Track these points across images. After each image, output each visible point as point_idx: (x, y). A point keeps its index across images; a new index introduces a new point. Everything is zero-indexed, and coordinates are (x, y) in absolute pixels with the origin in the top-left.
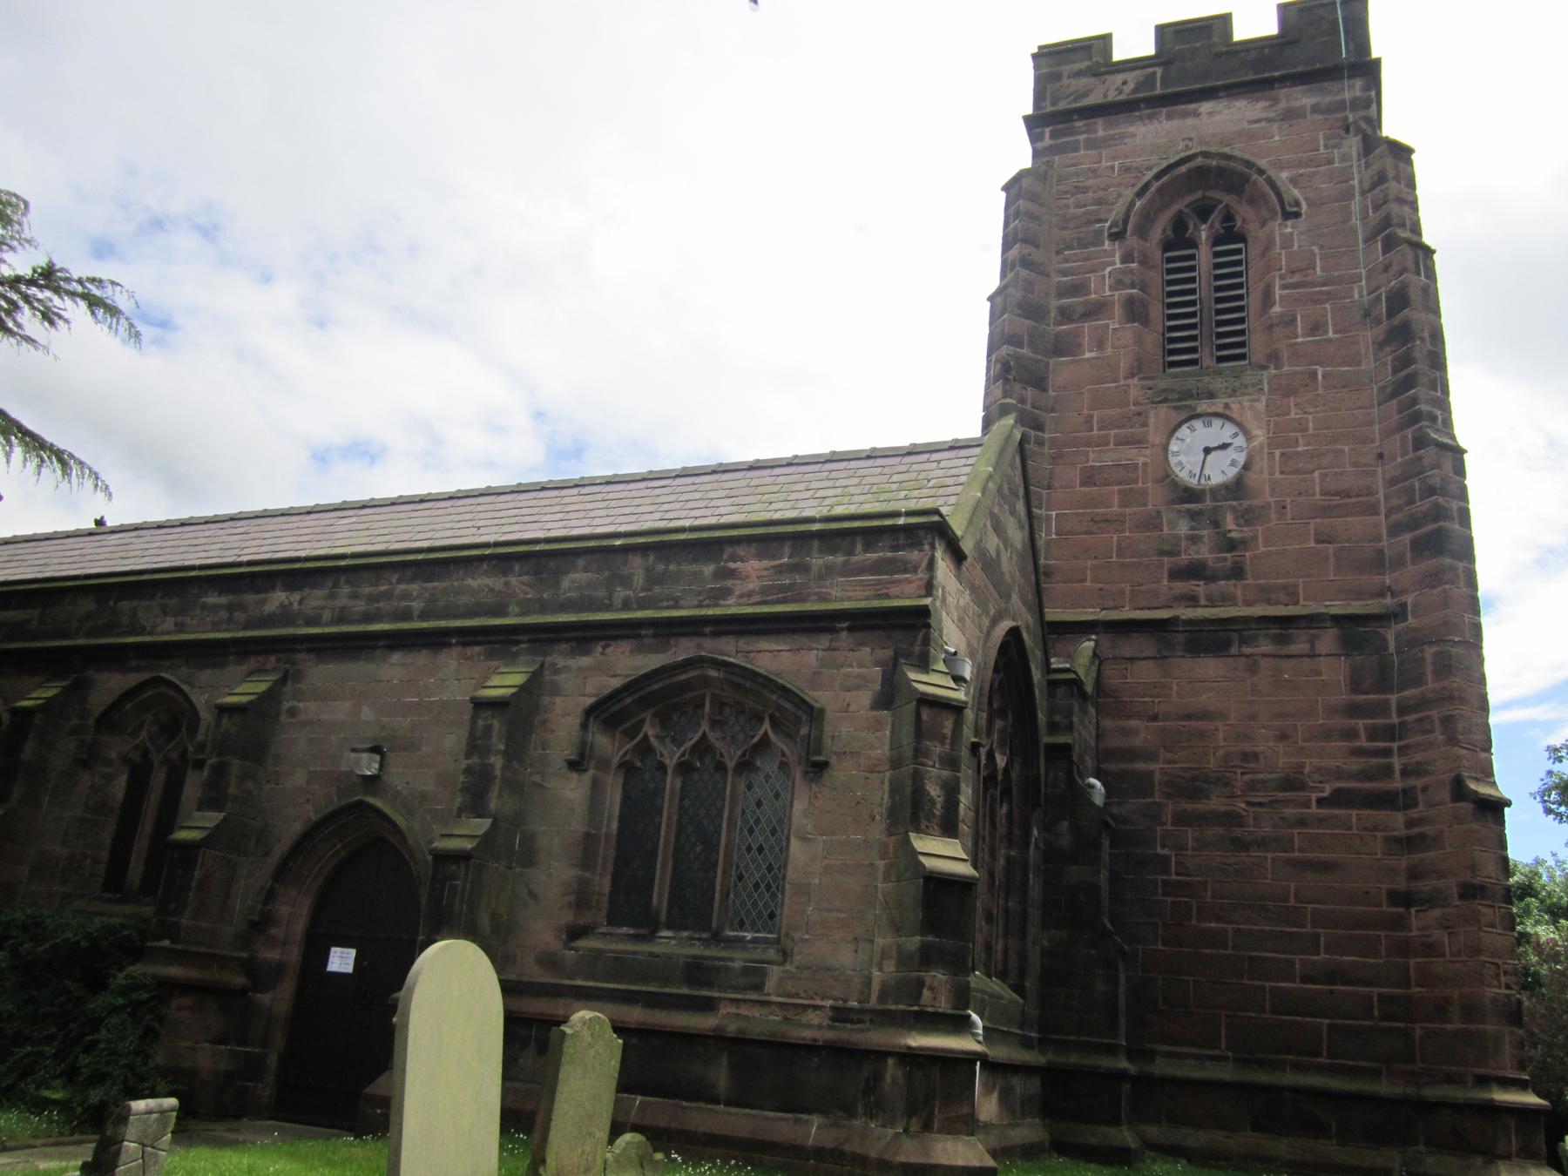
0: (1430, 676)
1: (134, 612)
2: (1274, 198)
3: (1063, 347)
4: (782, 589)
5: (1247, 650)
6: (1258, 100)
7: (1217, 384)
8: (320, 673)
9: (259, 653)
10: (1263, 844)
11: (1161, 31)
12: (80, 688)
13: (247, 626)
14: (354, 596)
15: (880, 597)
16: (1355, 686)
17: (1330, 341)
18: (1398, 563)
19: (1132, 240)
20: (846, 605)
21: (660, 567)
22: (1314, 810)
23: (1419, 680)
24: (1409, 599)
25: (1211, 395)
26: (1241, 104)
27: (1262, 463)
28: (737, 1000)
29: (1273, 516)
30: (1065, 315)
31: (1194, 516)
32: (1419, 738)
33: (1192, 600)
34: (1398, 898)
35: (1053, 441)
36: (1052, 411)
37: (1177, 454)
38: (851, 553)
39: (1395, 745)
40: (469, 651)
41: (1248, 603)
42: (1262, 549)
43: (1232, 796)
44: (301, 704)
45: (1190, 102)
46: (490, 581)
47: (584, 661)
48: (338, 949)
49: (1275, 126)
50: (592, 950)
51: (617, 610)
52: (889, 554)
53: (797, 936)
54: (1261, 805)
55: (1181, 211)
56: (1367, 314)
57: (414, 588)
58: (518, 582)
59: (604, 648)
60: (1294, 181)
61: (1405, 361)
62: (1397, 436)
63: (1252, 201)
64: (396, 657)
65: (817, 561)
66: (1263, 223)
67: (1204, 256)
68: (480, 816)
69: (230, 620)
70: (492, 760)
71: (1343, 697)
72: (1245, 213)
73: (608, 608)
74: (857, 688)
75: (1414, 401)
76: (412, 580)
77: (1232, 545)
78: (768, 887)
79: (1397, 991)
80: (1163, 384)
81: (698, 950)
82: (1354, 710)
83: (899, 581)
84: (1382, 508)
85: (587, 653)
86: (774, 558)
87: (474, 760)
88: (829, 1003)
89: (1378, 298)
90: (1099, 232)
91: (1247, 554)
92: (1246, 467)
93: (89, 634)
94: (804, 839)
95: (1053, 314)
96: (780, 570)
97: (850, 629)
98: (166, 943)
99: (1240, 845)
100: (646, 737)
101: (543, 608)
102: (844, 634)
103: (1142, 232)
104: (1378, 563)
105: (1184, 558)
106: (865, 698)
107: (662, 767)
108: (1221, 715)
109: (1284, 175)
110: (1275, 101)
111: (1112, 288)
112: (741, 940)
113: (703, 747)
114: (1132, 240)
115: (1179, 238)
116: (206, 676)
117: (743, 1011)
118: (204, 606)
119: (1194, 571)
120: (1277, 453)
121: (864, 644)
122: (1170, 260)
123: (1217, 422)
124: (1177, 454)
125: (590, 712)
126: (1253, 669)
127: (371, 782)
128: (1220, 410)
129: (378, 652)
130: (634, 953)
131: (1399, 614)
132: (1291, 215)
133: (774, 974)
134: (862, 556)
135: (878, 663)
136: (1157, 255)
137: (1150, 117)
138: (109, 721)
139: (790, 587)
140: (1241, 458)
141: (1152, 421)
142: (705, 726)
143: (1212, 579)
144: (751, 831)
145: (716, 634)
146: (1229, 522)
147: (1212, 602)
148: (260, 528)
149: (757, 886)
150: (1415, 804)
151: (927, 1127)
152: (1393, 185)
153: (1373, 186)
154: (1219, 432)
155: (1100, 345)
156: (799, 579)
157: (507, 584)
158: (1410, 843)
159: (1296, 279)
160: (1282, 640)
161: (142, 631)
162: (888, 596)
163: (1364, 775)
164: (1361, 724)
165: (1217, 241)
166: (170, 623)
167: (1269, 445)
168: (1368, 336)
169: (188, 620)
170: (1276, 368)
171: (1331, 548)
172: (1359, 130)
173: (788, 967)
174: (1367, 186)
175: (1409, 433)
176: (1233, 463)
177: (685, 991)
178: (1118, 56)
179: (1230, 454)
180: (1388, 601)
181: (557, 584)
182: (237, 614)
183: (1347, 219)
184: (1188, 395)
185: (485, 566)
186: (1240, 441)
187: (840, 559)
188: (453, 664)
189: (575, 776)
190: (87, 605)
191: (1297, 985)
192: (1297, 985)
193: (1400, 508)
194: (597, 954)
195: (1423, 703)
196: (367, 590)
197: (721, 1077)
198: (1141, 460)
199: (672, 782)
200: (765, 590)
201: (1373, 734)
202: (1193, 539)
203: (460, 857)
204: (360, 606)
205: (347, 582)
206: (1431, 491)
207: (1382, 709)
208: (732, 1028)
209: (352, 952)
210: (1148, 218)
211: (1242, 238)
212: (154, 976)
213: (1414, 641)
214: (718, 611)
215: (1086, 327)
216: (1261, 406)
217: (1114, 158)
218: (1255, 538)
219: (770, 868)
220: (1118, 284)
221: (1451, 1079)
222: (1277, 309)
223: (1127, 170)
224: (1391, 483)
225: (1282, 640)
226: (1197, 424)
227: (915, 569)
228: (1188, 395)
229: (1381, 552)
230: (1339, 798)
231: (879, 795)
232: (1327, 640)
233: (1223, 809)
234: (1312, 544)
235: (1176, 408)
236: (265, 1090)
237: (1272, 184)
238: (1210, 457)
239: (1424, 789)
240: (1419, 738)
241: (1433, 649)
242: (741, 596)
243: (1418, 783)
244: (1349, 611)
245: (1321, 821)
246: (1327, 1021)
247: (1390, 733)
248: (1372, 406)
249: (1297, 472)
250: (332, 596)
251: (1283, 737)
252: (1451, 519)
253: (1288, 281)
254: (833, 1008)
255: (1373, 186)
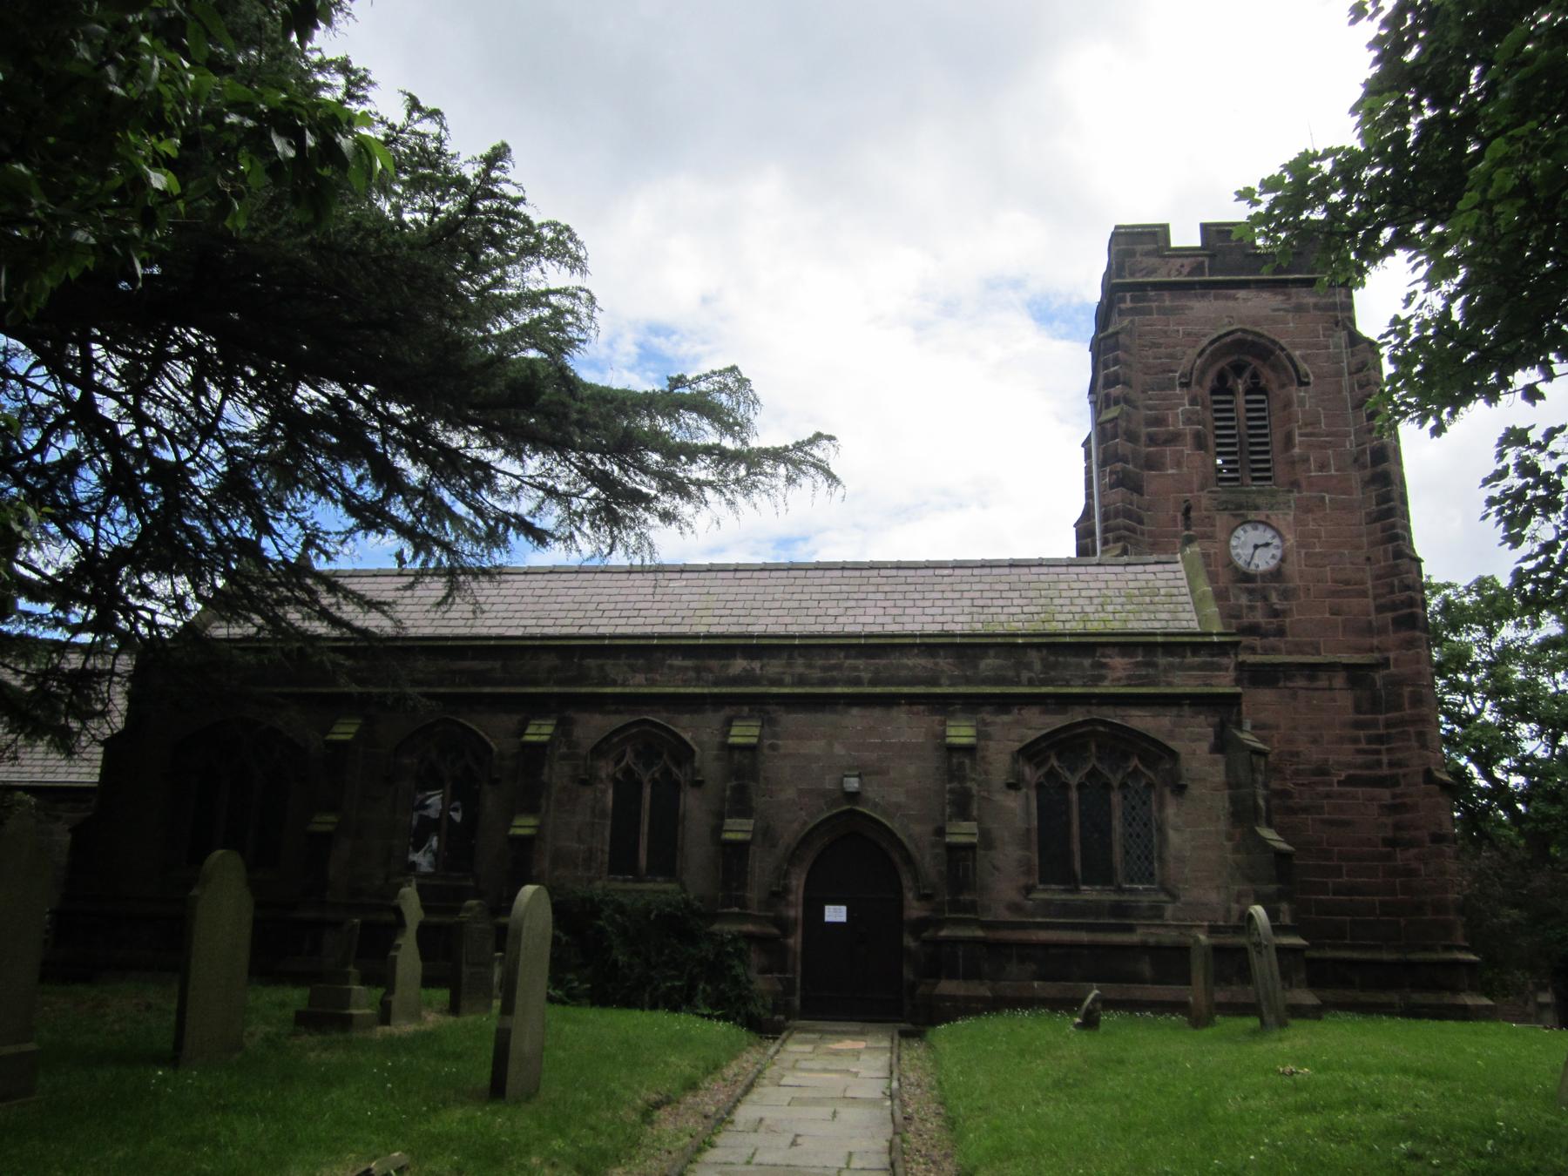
0: (1407, 706)
1: (601, 668)
2: (1291, 369)
3: (1152, 464)
4: (1140, 677)
5: (1291, 685)
6: (1276, 294)
7: (1260, 500)
8: (792, 720)
9: (731, 704)
10: (1305, 810)
11: (1205, 228)
12: (564, 726)
13: (716, 684)
14: (810, 666)
15: (1207, 685)
16: (1358, 709)
17: (1332, 476)
18: (1382, 631)
19: (1195, 388)
20: (1188, 690)
21: (1052, 659)
22: (1336, 788)
23: (1399, 708)
24: (1392, 655)
25: (1257, 508)
26: (1266, 295)
27: (1293, 558)
28: (1148, 925)
29: (1302, 595)
30: (1152, 440)
31: (1250, 592)
32: (1400, 744)
33: (1253, 650)
34: (1389, 842)
35: (1151, 535)
36: (1148, 510)
37: (1235, 547)
38: (1184, 657)
39: (1383, 747)
40: (915, 708)
41: (1289, 653)
42: (1297, 617)
43: (1285, 779)
44: (780, 742)
45: (1233, 288)
46: (922, 661)
47: (1006, 718)
48: (832, 908)
49: (1290, 316)
50: (1042, 900)
51: (1023, 685)
52: (1209, 659)
53: (1181, 886)
54: (1303, 785)
55: (1223, 368)
56: (1356, 460)
57: (861, 663)
58: (944, 663)
59: (1020, 710)
60: (1304, 358)
61: (1385, 498)
62: (1382, 548)
63: (1274, 368)
64: (855, 711)
65: (1162, 661)
66: (1283, 386)
67: (1240, 399)
68: (966, 820)
69: (698, 679)
70: (969, 784)
71: (1351, 716)
72: (1267, 374)
73: (1018, 684)
74: (1199, 740)
75: (1393, 526)
76: (856, 658)
77: (1276, 613)
78: (1146, 858)
79: (1387, 898)
80: (1224, 497)
81: (1114, 897)
82: (1357, 725)
83: (1217, 676)
84: (1370, 592)
85: (1008, 712)
86: (1132, 657)
87: (955, 785)
88: (1206, 923)
89: (1364, 451)
90: (1172, 379)
91: (1288, 620)
92: (1283, 560)
93: (559, 683)
94: (1177, 829)
95: (1143, 439)
96: (1137, 665)
97: (1190, 705)
98: (736, 910)
99: (1292, 811)
100: (1052, 767)
101: (968, 681)
102: (1186, 708)
103: (1200, 383)
104: (1369, 630)
105: (1245, 621)
106: (1204, 746)
107: (1065, 786)
108: (1277, 727)
109: (1298, 353)
110: (1289, 297)
111: (1184, 423)
112: (1137, 889)
113: (1093, 773)
114: (1195, 388)
115: (1222, 387)
116: (685, 719)
117: (1153, 930)
118: (671, 667)
119: (1253, 630)
120: (1303, 552)
121: (1200, 713)
122: (1216, 402)
123: (1261, 527)
124: (1235, 547)
125: (1021, 751)
126: (1294, 697)
127: (853, 797)
128: (1264, 519)
129: (840, 708)
130: (625, 881)
131: (1385, 664)
132: (1302, 384)
133: (1169, 910)
134: (1191, 659)
135: (1210, 725)
136: (1209, 398)
137: (1203, 296)
138: (598, 751)
139: (1146, 676)
140: (1278, 553)
141: (1218, 524)
142: (1094, 761)
143: (1264, 635)
144: (1130, 825)
145: (1100, 704)
146: (1274, 598)
147: (1266, 652)
148: (566, 584)
149: (1139, 858)
150: (1397, 784)
151: (1291, 986)
152: (1372, 372)
153: (1359, 370)
154: (1265, 535)
155: (1178, 464)
156: (1151, 671)
157: (936, 664)
158: (1393, 809)
159: (1308, 430)
160: (1311, 678)
161: (614, 683)
162: (1212, 686)
163: (1368, 766)
164: (1361, 733)
165: (1248, 392)
166: (640, 678)
167: (1298, 547)
168: (1356, 477)
169: (658, 677)
170: (1299, 492)
171: (1340, 618)
172: (1345, 327)
173: (1179, 904)
174: (1353, 370)
175: (1390, 547)
176: (1273, 557)
177: (1113, 921)
178: (1174, 243)
179: (1272, 551)
180: (1377, 655)
181: (976, 667)
182: (704, 674)
183: (1340, 391)
184: (1240, 507)
185: (916, 651)
186: (1276, 542)
187: (1177, 660)
188: (904, 717)
189: (1013, 792)
190: (549, 661)
191: (1330, 897)
192: (1330, 897)
193: (1384, 596)
194: (1048, 903)
195: (1402, 722)
196: (820, 662)
197: (1146, 968)
198: (1212, 551)
199: (1074, 795)
200: (1129, 677)
201: (1370, 740)
202: (1251, 608)
203: (971, 847)
204: (816, 674)
205: (800, 655)
206: (1408, 588)
207: (1374, 724)
208: (1152, 940)
209: (844, 909)
210: (1203, 372)
211: (1263, 391)
212: (740, 932)
213: (1396, 682)
214: (1096, 690)
215: (1168, 450)
216: (1290, 518)
217: (1180, 324)
218: (1291, 610)
219: (1146, 847)
220: (1188, 421)
221: (1426, 949)
222: (1297, 450)
223: (1189, 334)
224: (1378, 577)
225: (1311, 678)
226: (1248, 527)
227: (1227, 669)
228: (1240, 507)
229: (1370, 622)
230: (1351, 781)
231: (1222, 802)
232: (1339, 680)
233: (1280, 787)
234: (1327, 615)
235: (1234, 516)
236: (797, 1002)
237: (1290, 358)
238: (1258, 551)
239: (1405, 775)
240: (1400, 744)
241: (1410, 689)
242: (1113, 680)
243: (1401, 771)
244: (1353, 661)
245: (1341, 795)
246: (1348, 918)
247: (1380, 739)
248: (1361, 524)
249: (1315, 566)
250: (789, 665)
251: (1315, 741)
252: (1417, 606)
253: (1303, 431)
254: (1210, 926)
255: (1359, 370)
